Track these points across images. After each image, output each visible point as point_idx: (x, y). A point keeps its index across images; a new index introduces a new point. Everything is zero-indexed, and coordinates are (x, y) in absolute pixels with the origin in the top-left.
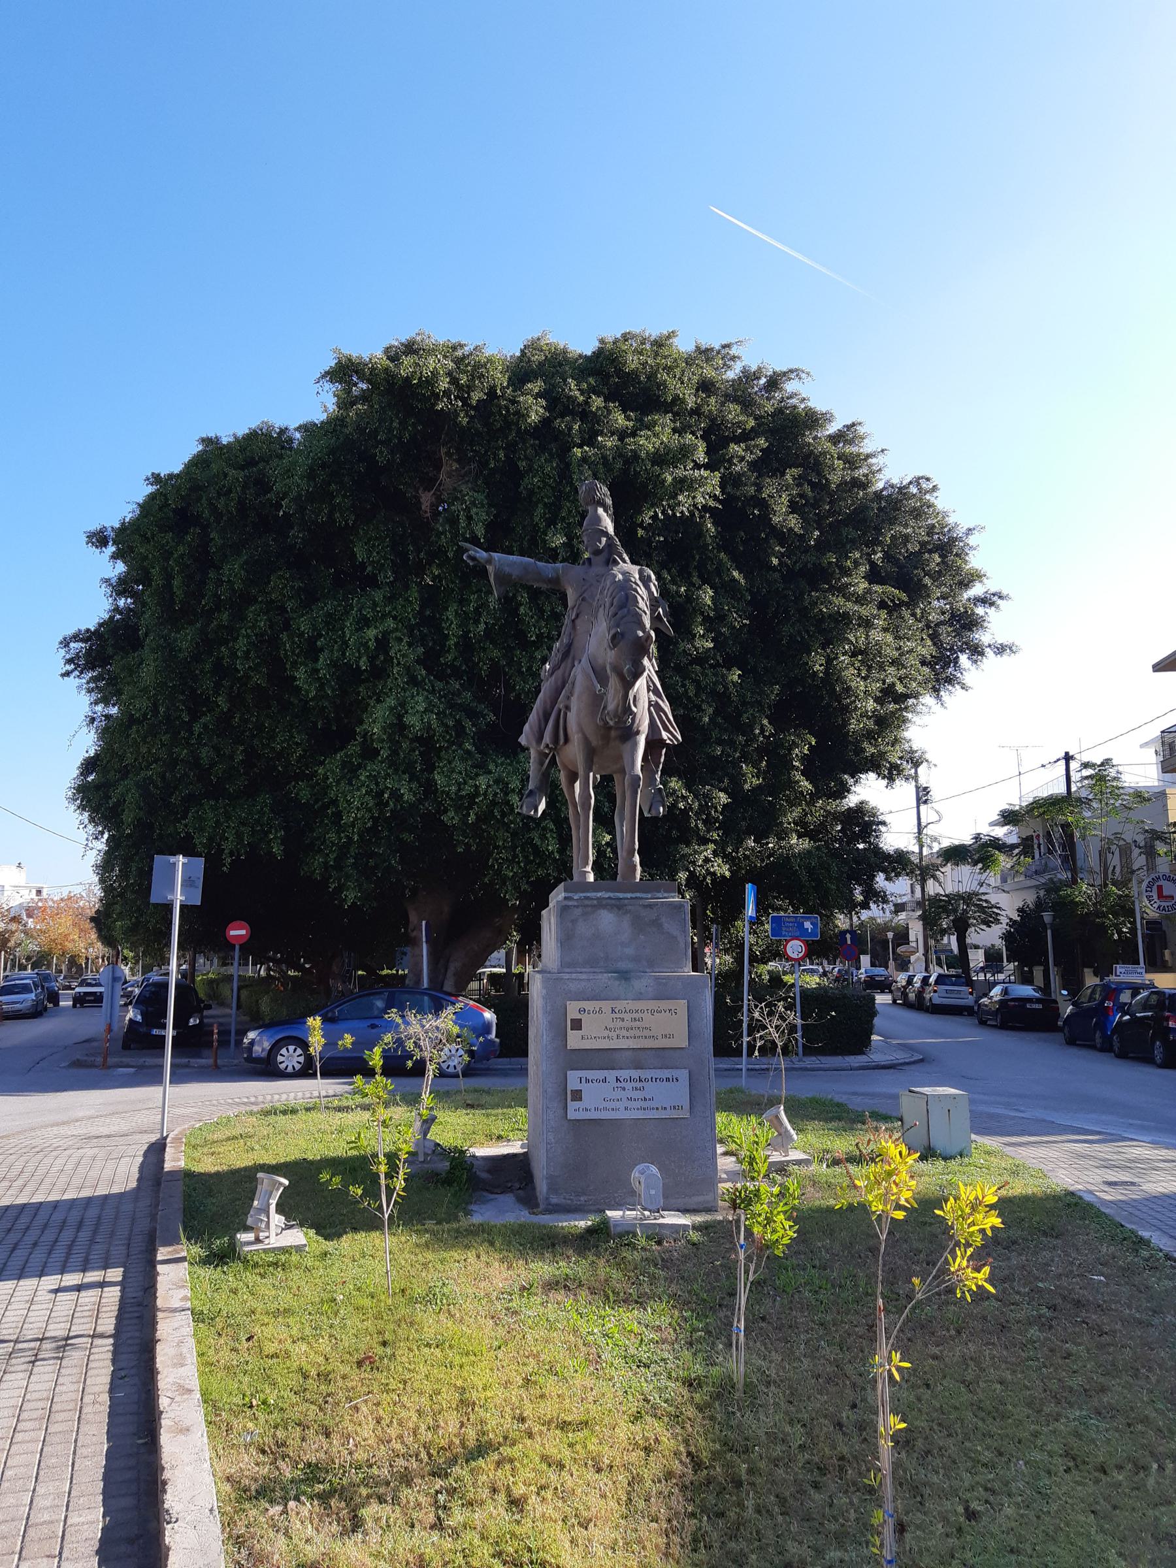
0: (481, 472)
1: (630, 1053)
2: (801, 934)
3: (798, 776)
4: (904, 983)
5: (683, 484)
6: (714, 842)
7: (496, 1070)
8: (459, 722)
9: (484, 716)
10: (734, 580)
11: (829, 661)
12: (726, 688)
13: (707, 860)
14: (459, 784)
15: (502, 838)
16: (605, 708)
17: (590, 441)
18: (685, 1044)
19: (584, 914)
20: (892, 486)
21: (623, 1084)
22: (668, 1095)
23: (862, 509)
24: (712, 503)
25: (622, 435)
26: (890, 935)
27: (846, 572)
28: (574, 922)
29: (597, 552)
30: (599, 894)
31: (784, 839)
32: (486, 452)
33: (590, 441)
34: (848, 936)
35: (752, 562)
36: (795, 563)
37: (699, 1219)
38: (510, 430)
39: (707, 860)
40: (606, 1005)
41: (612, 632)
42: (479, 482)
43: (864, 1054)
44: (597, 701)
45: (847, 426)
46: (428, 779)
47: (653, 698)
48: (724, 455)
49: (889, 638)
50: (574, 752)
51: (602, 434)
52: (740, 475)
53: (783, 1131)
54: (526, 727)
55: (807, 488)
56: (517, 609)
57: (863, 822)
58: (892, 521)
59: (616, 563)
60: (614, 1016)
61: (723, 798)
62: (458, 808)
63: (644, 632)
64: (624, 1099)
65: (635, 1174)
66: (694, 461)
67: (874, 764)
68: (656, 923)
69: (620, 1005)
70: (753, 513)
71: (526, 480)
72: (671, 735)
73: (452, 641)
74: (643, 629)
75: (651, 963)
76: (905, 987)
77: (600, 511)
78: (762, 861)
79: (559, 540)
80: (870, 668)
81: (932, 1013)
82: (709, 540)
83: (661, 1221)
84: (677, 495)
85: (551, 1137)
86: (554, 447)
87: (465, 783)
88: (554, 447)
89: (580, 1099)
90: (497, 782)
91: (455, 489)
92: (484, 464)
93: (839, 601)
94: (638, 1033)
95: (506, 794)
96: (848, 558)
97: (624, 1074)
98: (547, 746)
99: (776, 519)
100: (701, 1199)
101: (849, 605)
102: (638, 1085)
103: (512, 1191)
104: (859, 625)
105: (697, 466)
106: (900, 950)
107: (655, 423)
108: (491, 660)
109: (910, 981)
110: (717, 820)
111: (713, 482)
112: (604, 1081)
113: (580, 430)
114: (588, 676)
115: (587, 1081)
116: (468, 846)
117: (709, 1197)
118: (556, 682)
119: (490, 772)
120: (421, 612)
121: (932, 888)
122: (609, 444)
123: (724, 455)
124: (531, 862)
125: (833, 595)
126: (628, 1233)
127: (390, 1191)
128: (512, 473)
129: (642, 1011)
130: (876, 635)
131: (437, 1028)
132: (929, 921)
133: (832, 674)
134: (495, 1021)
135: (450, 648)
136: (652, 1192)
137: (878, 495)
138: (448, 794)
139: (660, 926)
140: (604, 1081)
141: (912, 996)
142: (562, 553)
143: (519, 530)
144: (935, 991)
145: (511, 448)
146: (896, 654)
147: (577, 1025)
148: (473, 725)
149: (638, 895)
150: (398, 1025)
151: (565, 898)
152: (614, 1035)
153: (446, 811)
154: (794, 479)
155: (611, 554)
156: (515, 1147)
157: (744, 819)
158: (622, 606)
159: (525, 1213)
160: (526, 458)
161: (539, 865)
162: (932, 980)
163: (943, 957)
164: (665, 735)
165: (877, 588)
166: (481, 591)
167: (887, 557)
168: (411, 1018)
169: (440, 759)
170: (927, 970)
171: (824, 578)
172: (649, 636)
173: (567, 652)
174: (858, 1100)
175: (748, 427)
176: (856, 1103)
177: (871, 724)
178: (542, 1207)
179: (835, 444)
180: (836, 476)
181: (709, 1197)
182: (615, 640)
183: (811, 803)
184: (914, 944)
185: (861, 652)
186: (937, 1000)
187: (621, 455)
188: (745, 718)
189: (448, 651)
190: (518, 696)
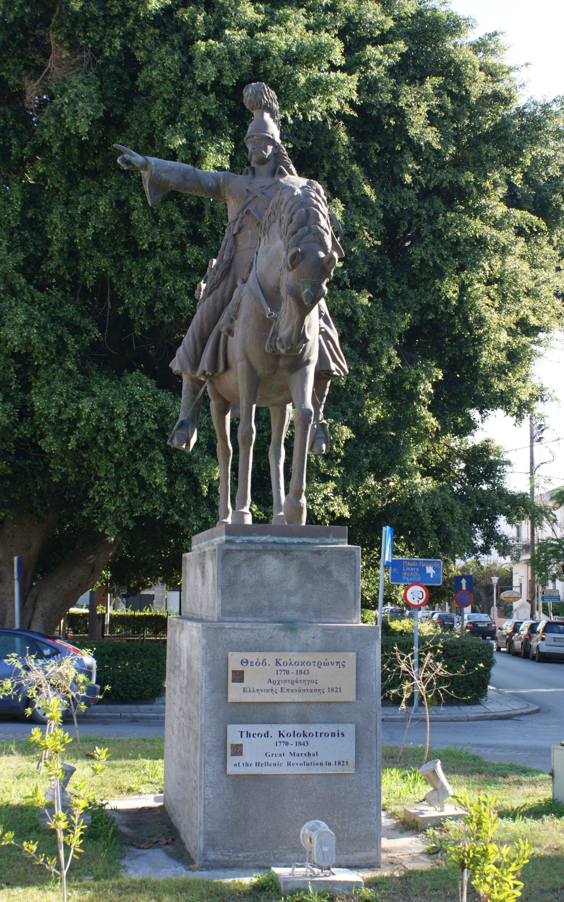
0: (94, 62)
1: (292, 708)
2: (421, 579)
3: (424, 412)
4: (509, 630)
5: (316, 86)
6: (335, 479)
7: (148, 718)
8: (60, 338)
9: (88, 332)
10: (365, 195)
11: (463, 288)
12: (354, 312)
13: (326, 498)
14: (59, 407)
15: (105, 468)
16: (275, 333)
17: (216, 32)
18: (352, 697)
19: (248, 559)
20: (535, 104)
21: (286, 739)
22: (334, 750)
23: (504, 125)
24: (347, 110)
25: (252, 29)
26: (495, 580)
27: (483, 192)
28: (237, 567)
29: (263, 161)
30: (263, 538)
31: (406, 477)
32: (102, 38)
33: (216, 32)
34: (464, 581)
35: (385, 176)
36: (429, 181)
37: (368, 875)
38: (128, 16)
39: (326, 498)
40: (271, 657)
41: (292, 251)
42: (90, 74)
43: (480, 704)
44: (266, 326)
45: (489, 35)
46: (23, 401)
47: (323, 325)
48: (360, 58)
49: (525, 267)
50: (236, 380)
51: (229, 27)
52: (376, 81)
53: (439, 786)
54: (180, 351)
55: (448, 101)
56: (129, 214)
57: (484, 463)
58: (535, 140)
59: (282, 174)
60: (279, 668)
61: (346, 433)
62: (58, 433)
63: (325, 251)
64: (287, 755)
65: (305, 830)
66: (329, 62)
67: (503, 400)
68: (325, 571)
69: (285, 657)
70: (389, 124)
71: (144, 72)
72: (340, 366)
73: (55, 248)
74: (325, 250)
75: (319, 613)
76: (511, 635)
77: (267, 116)
78: (384, 500)
79: (179, 141)
80: (504, 297)
81: (539, 661)
82: (341, 150)
83: (332, 878)
84: (310, 97)
85: (209, 793)
86: (176, 38)
87: (66, 406)
88: (176, 38)
89: (241, 753)
90: (102, 406)
91: (64, 80)
92: (97, 53)
93: (476, 224)
94: (303, 686)
95: (111, 420)
96: (486, 178)
97: (287, 728)
98: (204, 373)
99: (412, 132)
100: (364, 855)
101: (487, 229)
102: (302, 739)
103: (159, 847)
104: (495, 251)
105: (333, 68)
106: (505, 595)
107: (286, 18)
108: (98, 269)
109: (516, 629)
110: (338, 456)
111: (349, 85)
112: (267, 735)
113: (205, 23)
114: (257, 299)
115: (248, 735)
116: (65, 476)
117: (372, 854)
118: (215, 301)
119: (94, 395)
120: (22, 215)
121: (545, 532)
122: (238, 38)
123: (360, 58)
124: (136, 496)
125: (470, 216)
126: (299, 890)
127: (67, 848)
128: (131, 64)
129: (309, 664)
130: (512, 263)
131: (61, 674)
132: (538, 566)
133: (464, 303)
134: (95, 666)
135: (53, 255)
136: (326, 849)
137: (520, 113)
138: (46, 418)
139: (329, 573)
140: (267, 735)
141: (518, 644)
142: (182, 155)
143: (135, 126)
144: (543, 639)
145: (129, 36)
146: (531, 285)
147: (239, 677)
148: (76, 342)
149: (305, 540)
150: (18, 671)
151: (227, 542)
152: (278, 687)
153: (43, 436)
154: (434, 88)
155: (277, 164)
156: (148, 800)
157: (367, 455)
158: (303, 223)
159: (181, 869)
160: (145, 48)
161: (145, 499)
162: (540, 628)
163: (550, 604)
164: (333, 366)
165: (518, 213)
166: (89, 192)
167: (526, 179)
168: (31, 661)
169: (37, 377)
170: (532, 616)
171: (456, 196)
172: (332, 258)
173: (228, 269)
174: (489, 752)
175: (387, 27)
176: (488, 755)
177: (502, 357)
178: (198, 863)
179: (476, 53)
180: (478, 86)
181: (372, 854)
182: (295, 260)
183: (436, 439)
184: (518, 590)
185: (496, 281)
186: (544, 648)
187: (250, 51)
188: (371, 349)
189: (51, 258)
190: (126, 311)
